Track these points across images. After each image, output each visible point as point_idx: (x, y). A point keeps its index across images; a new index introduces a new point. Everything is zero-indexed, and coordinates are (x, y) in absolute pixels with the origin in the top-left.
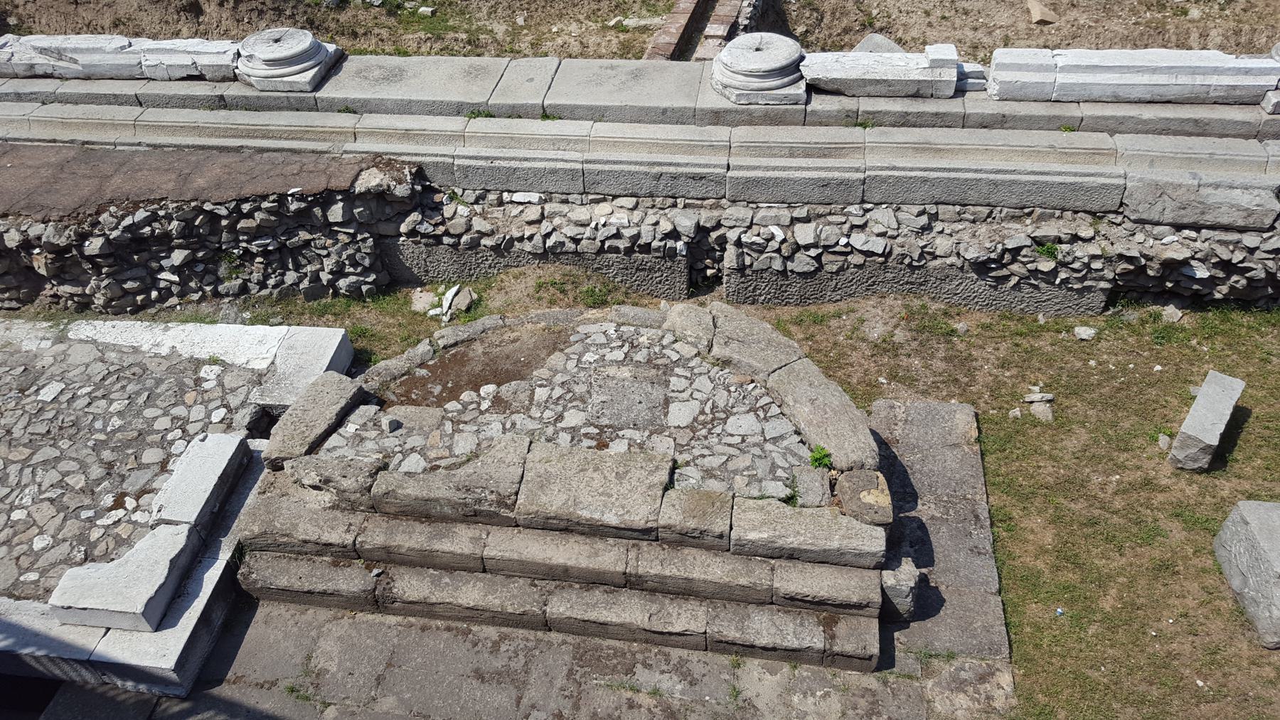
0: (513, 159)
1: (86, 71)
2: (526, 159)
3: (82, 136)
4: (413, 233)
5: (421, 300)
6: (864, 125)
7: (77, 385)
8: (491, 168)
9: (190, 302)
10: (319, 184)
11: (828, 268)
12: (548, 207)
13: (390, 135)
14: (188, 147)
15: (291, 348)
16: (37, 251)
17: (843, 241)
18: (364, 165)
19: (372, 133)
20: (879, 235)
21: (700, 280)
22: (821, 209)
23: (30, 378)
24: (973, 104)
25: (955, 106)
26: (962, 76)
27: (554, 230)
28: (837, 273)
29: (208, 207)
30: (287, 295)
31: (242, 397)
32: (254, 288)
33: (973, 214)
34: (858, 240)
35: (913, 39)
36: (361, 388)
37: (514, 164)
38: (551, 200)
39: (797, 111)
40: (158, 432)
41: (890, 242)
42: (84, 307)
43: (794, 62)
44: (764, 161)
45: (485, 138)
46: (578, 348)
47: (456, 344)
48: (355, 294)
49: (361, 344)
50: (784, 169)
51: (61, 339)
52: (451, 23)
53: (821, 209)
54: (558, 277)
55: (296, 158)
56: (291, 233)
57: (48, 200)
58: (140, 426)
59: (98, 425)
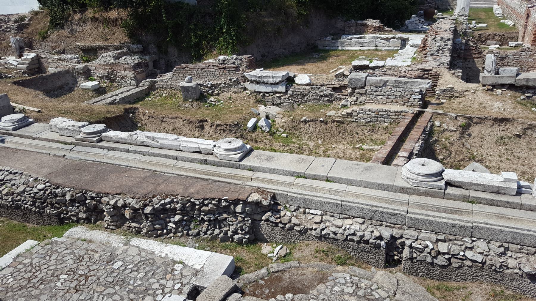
0: (312, 196)
1: (161, 146)
2: (317, 197)
3: (154, 168)
4: (267, 220)
5: (266, 249)
6: (472, 202)
7: (128, 264)
8: (302, 198)
9: (177, 236)
10: (234, 196)
11: (454, 265)
12: (324, 217)
13: (265, 181)
14: (190, 177)
15: (211, 262)
16: (128, 208)
17: (462, 253)
18: (253, 191)
19: (258, 179)
20: (479, 253)
21: (391, 260)
22: (451, 237)
23: (112, 258)
24: (524, 199)
25: (516, 200)
26: (520, 187)
27: (326, 227)
28: (458, 268)
29: (192, 200)
30: (214, 239)
31: (188, 280)
32: (202, 234)
33: (527, 250)
34: (469, 254)
35: (493, 166)
36: (235, 285)
37: (312, 198)
38: (326, 215)
39: (441, 192)
40: (153, 289)
41: (485, 258)
42: (138, 232)
43: (440, 172)
44: (425, 212)
45: (302, 186)
46: (331, 283)
47: (277, 272)
48: (240, 242)
49: (239, 264)
50: (434, 217)
51: (127, 244)
52: (293, 140)
53: (451, 237)
54: (325, 249)
55: (228, 185)
56: (221, 214)
57: (136, 190)
58: (147, 286)
59: (132, 282)
